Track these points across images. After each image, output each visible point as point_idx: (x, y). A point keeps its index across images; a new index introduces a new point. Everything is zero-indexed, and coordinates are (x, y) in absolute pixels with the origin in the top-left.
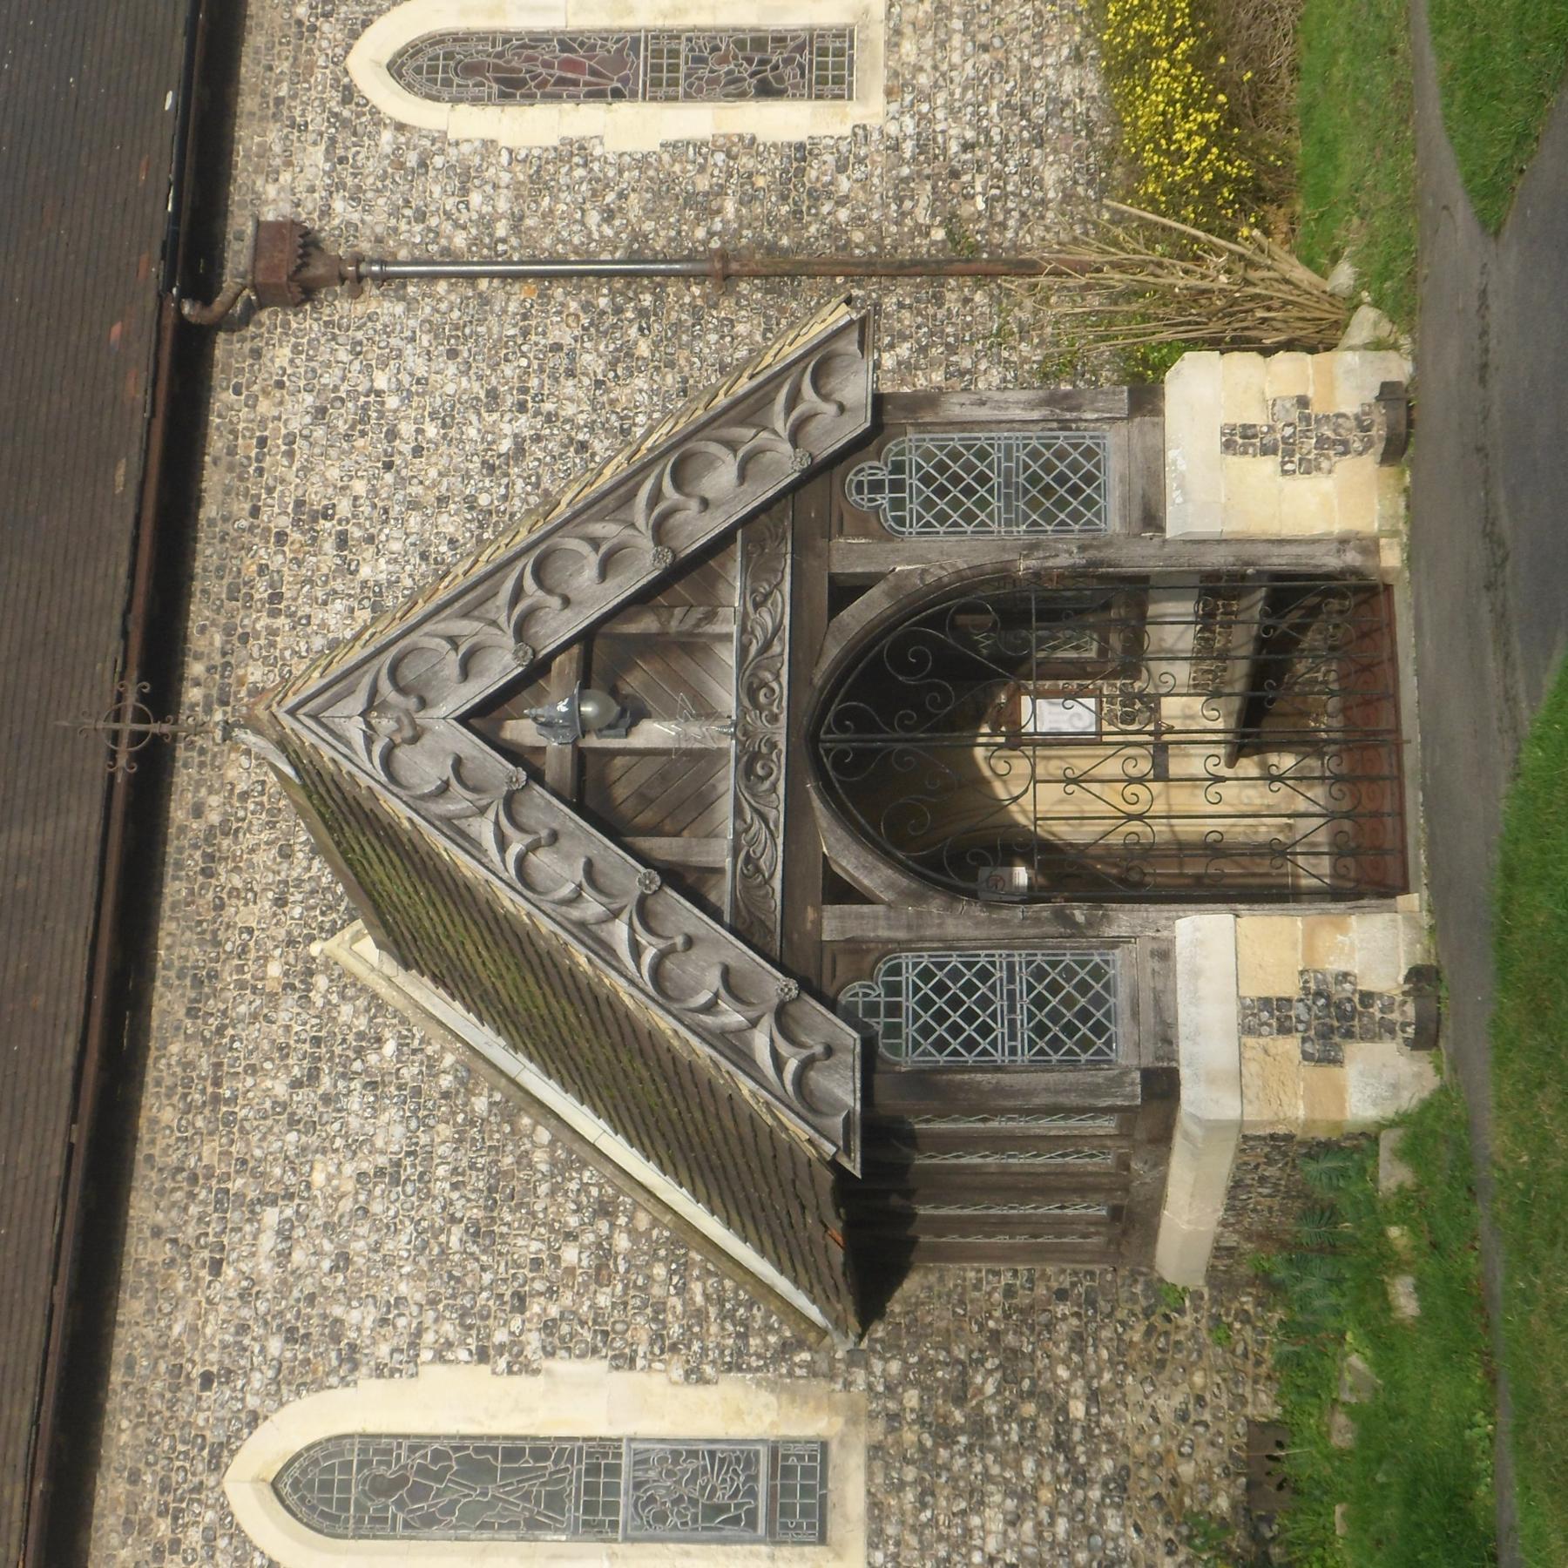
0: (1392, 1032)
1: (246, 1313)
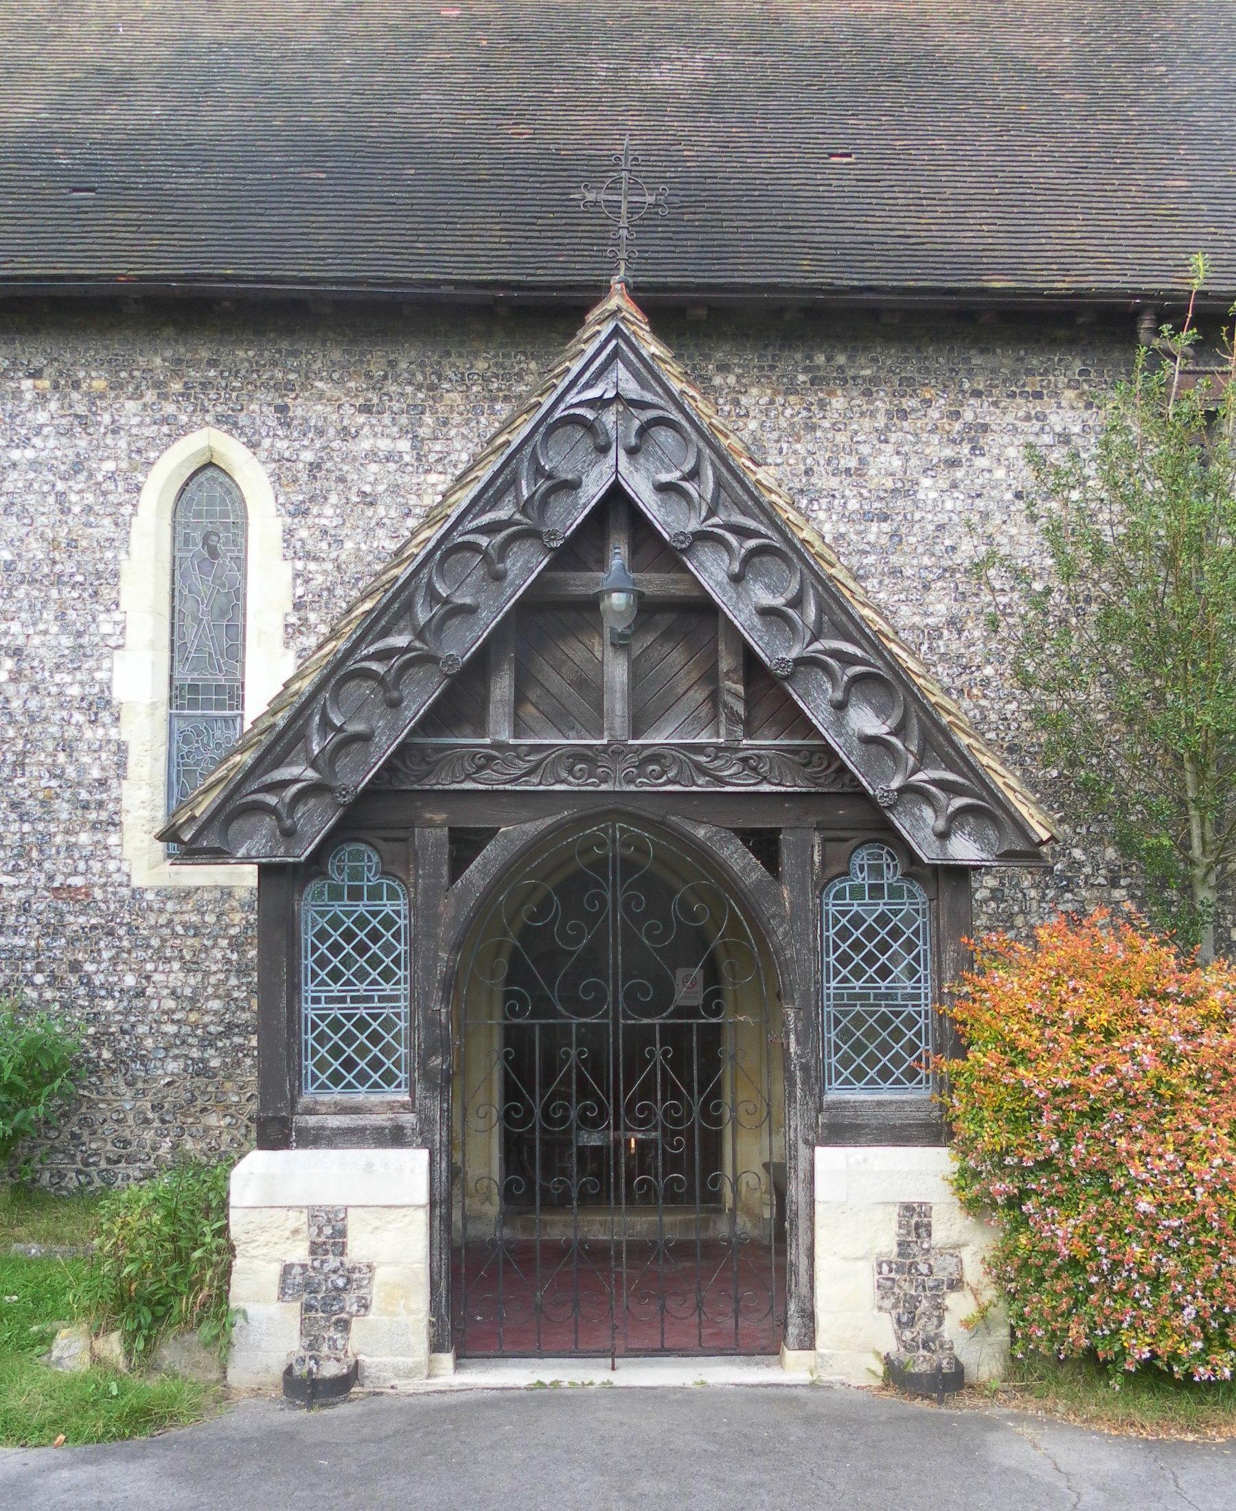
0: (311, 1347)
1: (332, 432)
